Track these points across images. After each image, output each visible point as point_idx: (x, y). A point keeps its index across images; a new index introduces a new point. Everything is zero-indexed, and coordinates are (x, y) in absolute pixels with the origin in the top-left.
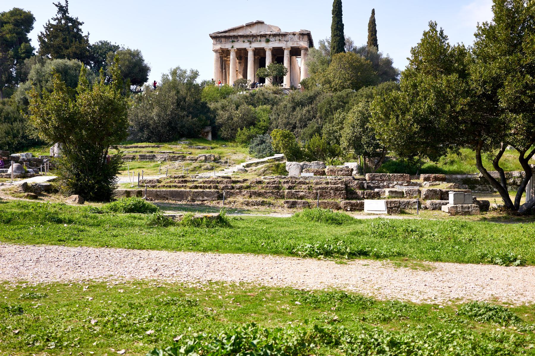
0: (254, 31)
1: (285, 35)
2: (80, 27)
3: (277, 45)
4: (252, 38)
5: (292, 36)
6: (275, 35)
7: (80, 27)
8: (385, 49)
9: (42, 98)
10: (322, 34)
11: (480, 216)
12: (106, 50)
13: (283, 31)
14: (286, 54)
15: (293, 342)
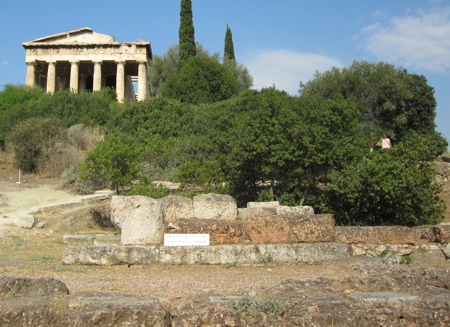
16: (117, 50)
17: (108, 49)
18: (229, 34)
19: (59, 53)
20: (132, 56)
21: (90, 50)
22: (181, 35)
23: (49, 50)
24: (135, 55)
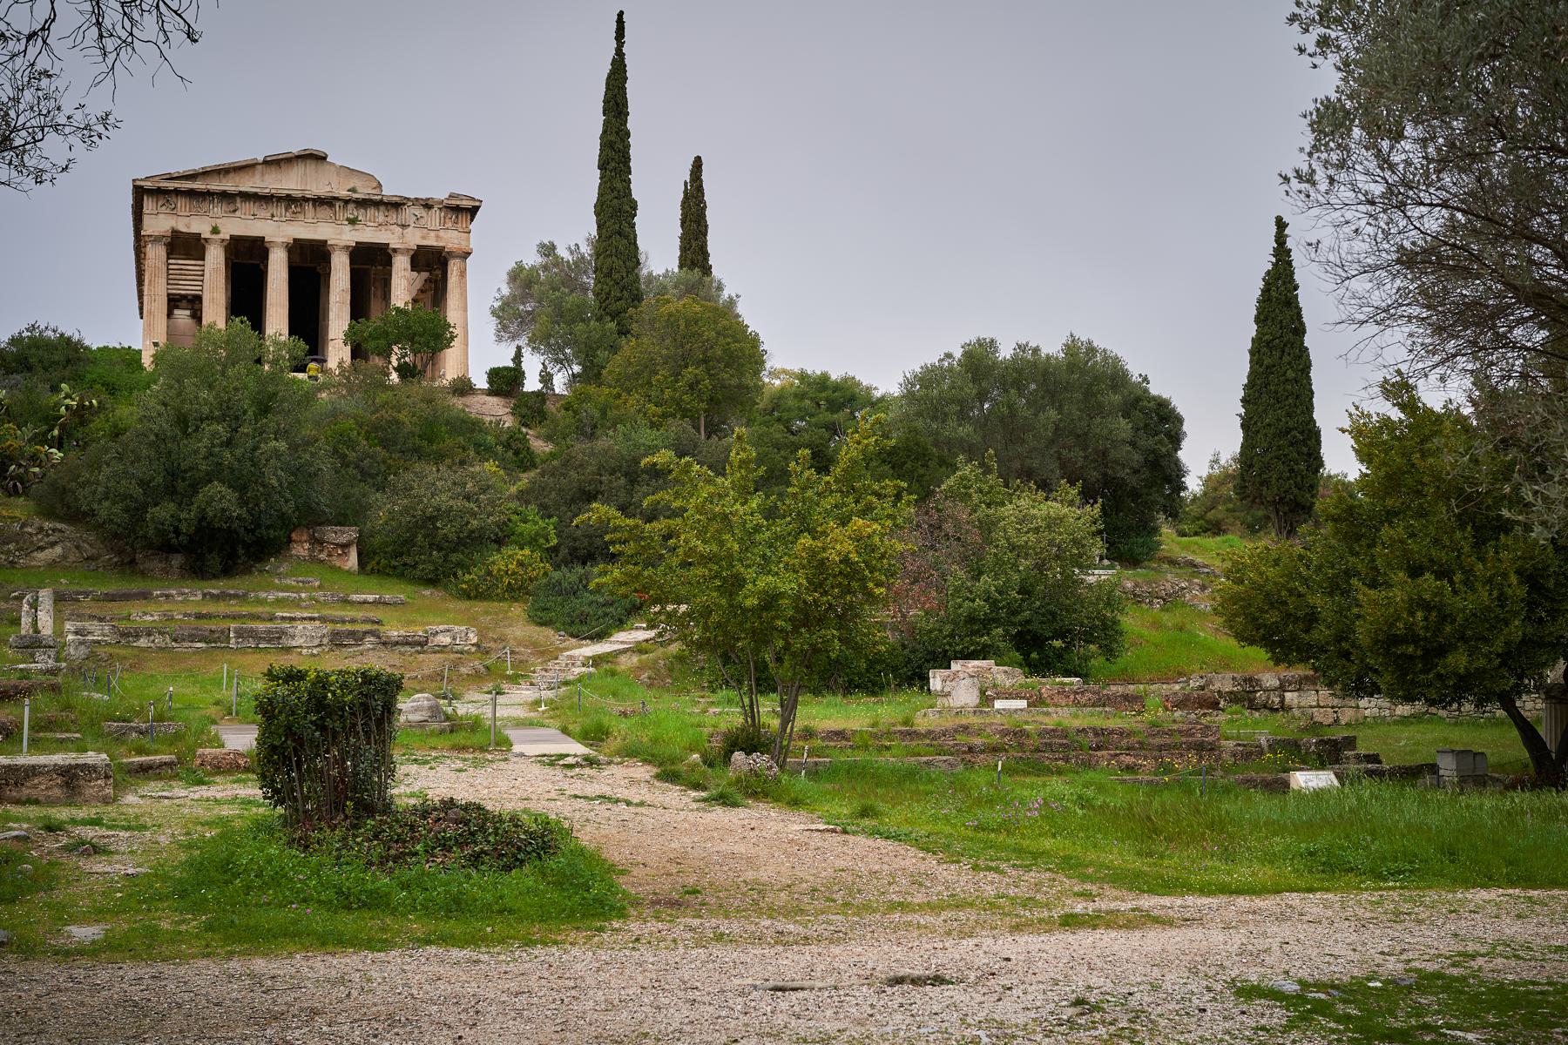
1: (396, 205)
3: (369, 233)
5: (419, 211)
6: (364, 204)
11: (722, 713)
13: (390, 191)
16: (393, 217)
17: (371, 212)
18: (698, 164)
19: (238, 214)
20: (432, 234)
21: (325, 212)
22: (600, 209)
23: (205, 206)
24: (442, 233)
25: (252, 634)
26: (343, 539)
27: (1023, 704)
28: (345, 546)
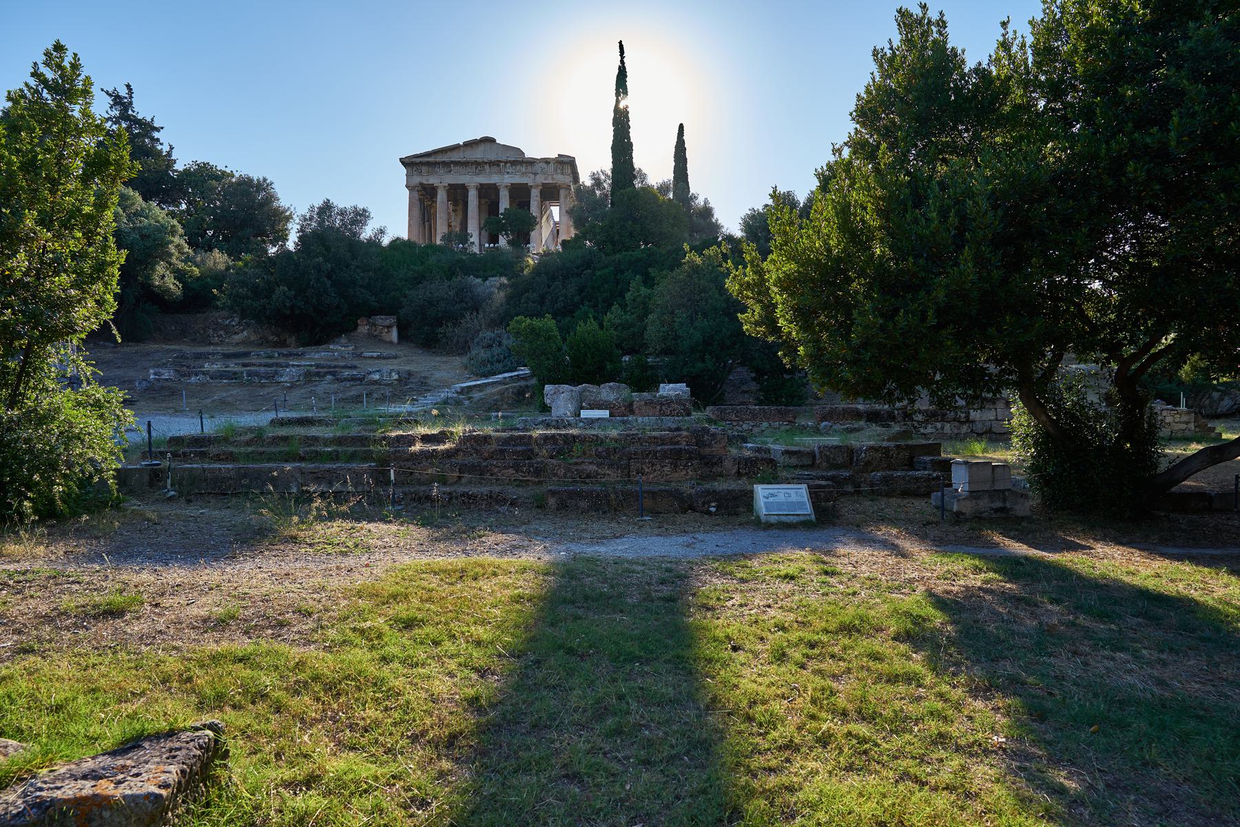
0: (477, 154)
2: (156, 135)
3: (517, 179)
4: (479, 165)
5: (544, 165)
6: (514, 163)
7: (156, 135)
8: (701, 187)
9: (741, 606)
10: (594, 162)
12: (203, 176)
14: (535, 194)
15: (738, 698)
16: (530, 169)
21: (495, 168)
25: (256, 374)
26: (387, 323)
27: (605, 414)
28: (389, 327)
